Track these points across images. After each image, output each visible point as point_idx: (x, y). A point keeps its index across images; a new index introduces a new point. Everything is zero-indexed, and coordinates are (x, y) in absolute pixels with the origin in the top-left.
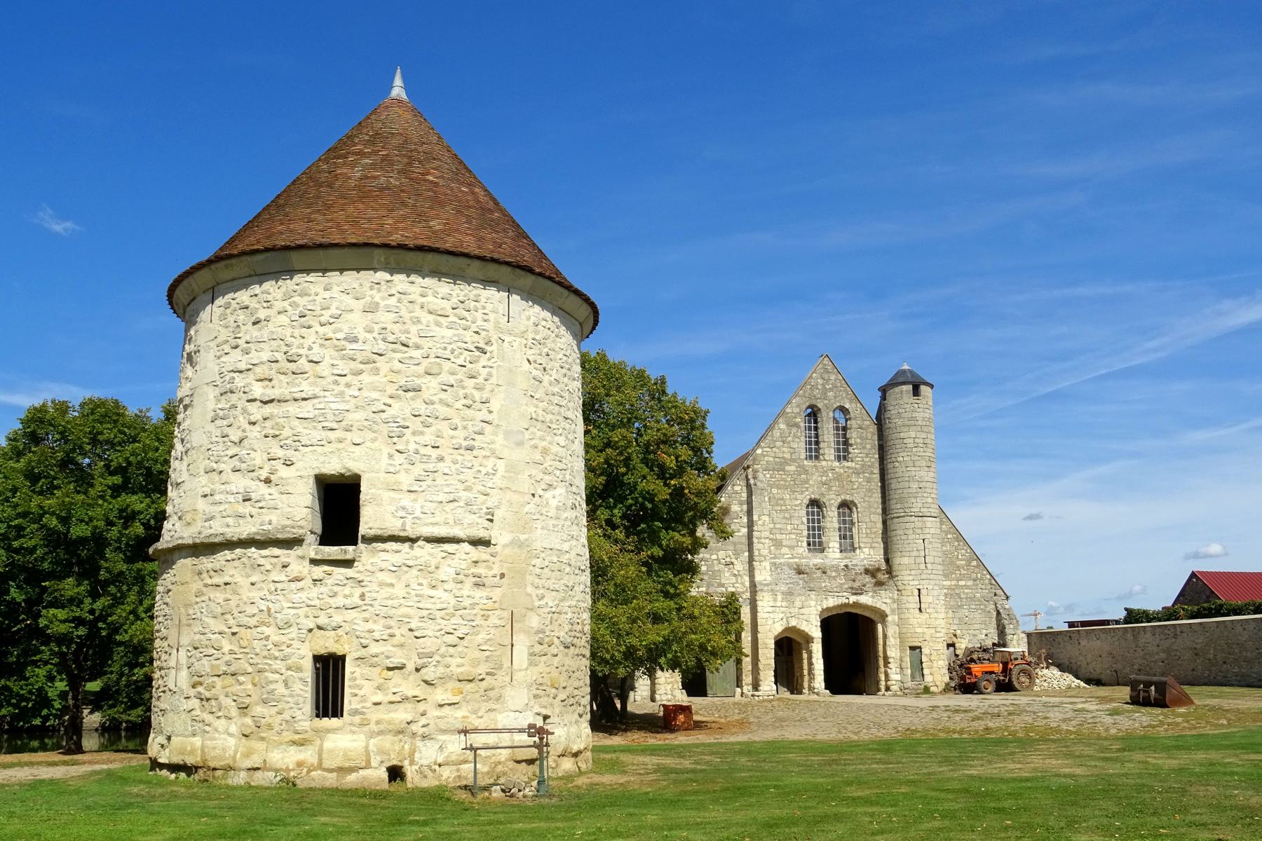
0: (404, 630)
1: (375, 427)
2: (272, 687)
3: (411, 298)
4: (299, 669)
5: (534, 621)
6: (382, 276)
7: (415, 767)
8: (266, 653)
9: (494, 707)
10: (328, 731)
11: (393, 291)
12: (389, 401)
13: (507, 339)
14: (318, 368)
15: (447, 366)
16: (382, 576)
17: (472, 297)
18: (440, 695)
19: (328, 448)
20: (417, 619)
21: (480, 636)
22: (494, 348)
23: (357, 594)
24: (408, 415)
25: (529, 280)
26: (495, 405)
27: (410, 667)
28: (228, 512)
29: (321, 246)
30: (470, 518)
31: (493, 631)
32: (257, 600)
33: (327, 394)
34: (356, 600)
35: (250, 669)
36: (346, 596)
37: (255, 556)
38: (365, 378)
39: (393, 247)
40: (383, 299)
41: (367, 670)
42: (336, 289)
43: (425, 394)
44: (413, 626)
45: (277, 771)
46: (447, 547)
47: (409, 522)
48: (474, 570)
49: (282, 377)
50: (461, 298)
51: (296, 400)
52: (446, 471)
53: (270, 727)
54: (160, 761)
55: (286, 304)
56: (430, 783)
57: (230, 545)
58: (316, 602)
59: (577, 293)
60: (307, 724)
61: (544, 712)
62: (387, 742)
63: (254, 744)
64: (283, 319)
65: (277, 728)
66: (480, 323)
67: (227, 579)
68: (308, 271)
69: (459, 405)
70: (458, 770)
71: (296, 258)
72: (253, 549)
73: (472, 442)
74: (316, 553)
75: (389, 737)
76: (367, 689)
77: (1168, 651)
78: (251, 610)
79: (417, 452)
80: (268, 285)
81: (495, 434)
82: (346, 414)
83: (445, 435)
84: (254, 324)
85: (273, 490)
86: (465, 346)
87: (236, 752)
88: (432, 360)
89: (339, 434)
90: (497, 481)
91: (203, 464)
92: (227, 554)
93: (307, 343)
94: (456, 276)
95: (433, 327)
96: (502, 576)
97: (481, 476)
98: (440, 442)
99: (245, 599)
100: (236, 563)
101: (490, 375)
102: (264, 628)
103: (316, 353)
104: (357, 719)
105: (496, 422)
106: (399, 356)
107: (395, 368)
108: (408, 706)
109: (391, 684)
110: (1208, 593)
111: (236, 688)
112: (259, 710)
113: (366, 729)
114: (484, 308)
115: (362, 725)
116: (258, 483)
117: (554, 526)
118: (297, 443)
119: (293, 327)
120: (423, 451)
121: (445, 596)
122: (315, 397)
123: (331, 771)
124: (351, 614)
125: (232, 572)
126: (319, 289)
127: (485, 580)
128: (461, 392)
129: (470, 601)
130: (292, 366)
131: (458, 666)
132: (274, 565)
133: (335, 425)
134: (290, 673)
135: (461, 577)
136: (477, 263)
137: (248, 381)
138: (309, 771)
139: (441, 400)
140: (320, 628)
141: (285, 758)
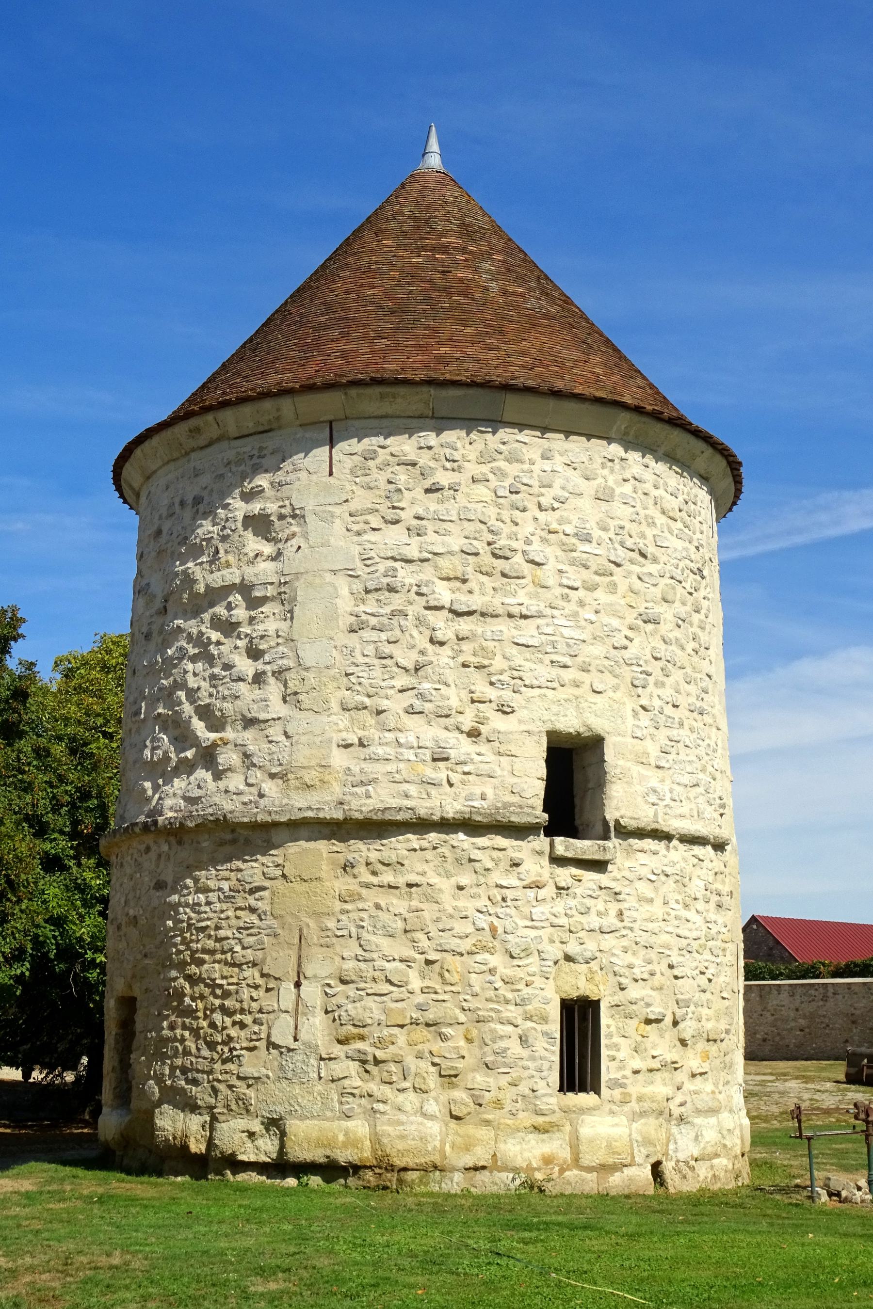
0: (664, 967)
1: (618, 671)
2: (503, 1044)
4: (544, 1019)
6: (616, 450)
8: (492, 993)
10: (583, 1111)
11: (628, 475)
12: (630, 634)
14: (539, 571)
23: (613, 913)
28: (405, 775)
29: (556, 394)
33: (556, 612)
34: (611, 921)
35: (462, 1018)
37: (466, 846)
45: (516, 1170)
47: (661, 810)
49: (484, 579)
51: (510, 616)
53: (498, 1104)
54: (242, 1157)
55: (485, 469)
56: (690, 1186)
57: (421, 825)
58: (563, 921)
60: (553, 1100)
62: (650, 1126)
63: (469, 1129)
64: (482, 491)
67: (413, 878)
68: (521, 426)
70: (712, 1167)
71: (512, 404)
72: (461, 836)
74: (567, 848)
75: (652, 1121)
77: (812, 1017)
78: (461, 927)
80: (451, 436)
82: (583, 646)
84: (428, 491)
85: (484, 748)
87: (443, 1143)
89: (567, 675)
91: (335, 697)
92: (413, 840)
99: (451, 911)
100: (429, 855)
102: (487, 956)
103: (536, 550)
104: (617, 1093)
106: (636, 569)
110: (771, 943)
111: (437, 1046)
112: (480, 1079)
113: (626, 1108)
116: (456, 734)
119: (499, 506)
122: (540, 615)
123: (589, 1169)
124: (608, 942)
125: (420, 867)
126: (535, 455)
130: (500, 564)
132: (497, 862)
133: (567, 660)
134: (529, 1024)
137: (423, 577)
138: (562, 1171)
140: (568, 958)
141: (526, 1151)
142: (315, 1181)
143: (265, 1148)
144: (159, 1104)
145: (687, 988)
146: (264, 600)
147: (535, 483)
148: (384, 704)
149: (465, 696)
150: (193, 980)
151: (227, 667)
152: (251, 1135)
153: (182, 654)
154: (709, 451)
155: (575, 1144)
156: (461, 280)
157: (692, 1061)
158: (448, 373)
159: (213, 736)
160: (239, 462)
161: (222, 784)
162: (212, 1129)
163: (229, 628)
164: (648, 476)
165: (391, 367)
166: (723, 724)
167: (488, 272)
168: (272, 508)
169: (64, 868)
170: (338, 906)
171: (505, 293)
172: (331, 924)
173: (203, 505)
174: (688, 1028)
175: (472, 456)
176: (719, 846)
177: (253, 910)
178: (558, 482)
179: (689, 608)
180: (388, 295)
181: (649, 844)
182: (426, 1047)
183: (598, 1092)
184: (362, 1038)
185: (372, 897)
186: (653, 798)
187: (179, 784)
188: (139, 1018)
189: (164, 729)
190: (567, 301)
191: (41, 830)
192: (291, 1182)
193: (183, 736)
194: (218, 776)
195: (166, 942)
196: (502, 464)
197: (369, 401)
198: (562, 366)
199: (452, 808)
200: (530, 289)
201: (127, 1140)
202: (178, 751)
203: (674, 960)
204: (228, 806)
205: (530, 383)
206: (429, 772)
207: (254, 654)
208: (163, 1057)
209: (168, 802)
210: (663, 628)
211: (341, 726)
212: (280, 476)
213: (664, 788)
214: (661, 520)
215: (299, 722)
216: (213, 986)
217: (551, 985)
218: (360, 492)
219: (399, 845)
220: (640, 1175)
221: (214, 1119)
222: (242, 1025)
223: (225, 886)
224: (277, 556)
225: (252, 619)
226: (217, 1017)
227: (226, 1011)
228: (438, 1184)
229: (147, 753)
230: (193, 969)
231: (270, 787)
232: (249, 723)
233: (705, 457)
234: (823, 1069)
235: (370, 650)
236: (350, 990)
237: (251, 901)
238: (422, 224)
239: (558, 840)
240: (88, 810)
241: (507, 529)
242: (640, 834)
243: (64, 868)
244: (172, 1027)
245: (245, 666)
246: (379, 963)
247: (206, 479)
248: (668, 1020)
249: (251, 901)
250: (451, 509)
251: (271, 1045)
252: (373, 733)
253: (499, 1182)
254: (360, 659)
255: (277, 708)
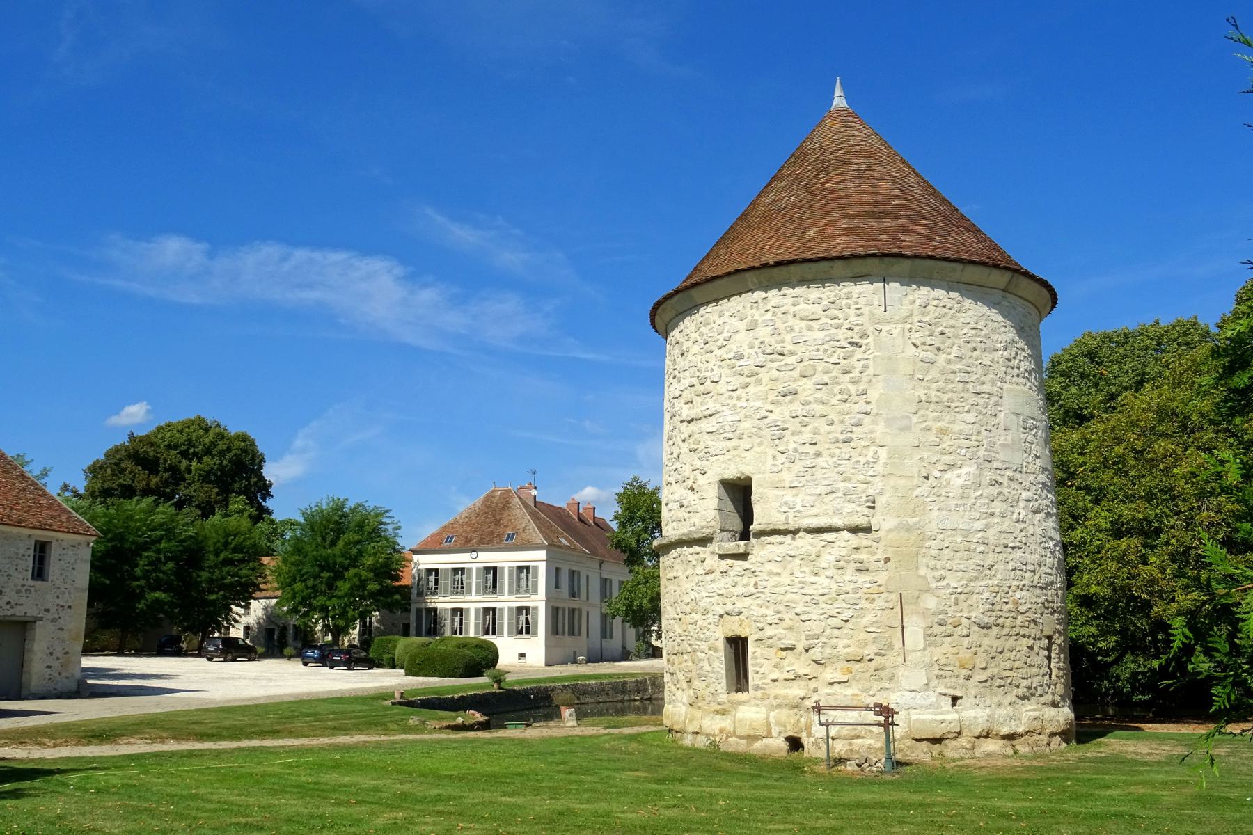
0: (792, 615)
1: (761, 433)
3: (783, 309)
5: (931, 603)
6: (759, 294)
7: (812, 739)
9: (887, 686)
10: (740, 703)
13: (885, 328)
14: (718, 386)
15: (820, 366)
16: (769, 567)
17: (843, 295)
18: (829, 674)
19: (727, 457)
20: (801, 604)
21: (865, 619)
22: (870, 339)
24: (788, 417)
25: (906, 264)
26: (873, 395)
27: (800, 647)
30: (849, 507)
31: (879, 613)
34: (752, 589)
36: (744, 586)
38: (752, 390)
39: (758, 268)
40: (761, 315)
41: (765, 651)
42: (727, 314)
43: (802, 396)
44: (798, 610)
45: (708, 735)
46: (826, 536)
47: (791, 515)
48: (855, 556)
50: (831, 299)
52: (824, 465)
58: (723, 591)
61: (953, 692)
62: (784, 714)
65: (707, 699)
66: (853, 318)
68: (706, 304)
69: (835, 401)
70: (850, 744)
73: (850, 435)
75: (785, 711)
76: (766, 667)
79: (796, 451)
81: (874, 423)
83: (822, 431)
85: (696, 497)
86: (837, 344)
88: (806, 363)
90: (879, 468)
94: (823, 280)
95: (805, 332)
96: (887, 560)
97: (860, 466)
98: (817, 438)
101: (866, 367)
104: (759, 693)
105: (875, 411)
106: (776, 365)
107: (774, 377)
108: (802, 683)
109: (785, 663)
113: (766, 702)
114: (857, 303)
115: (763, 699)
117: (957, 506)
118: (707, 455)
120: (801, 449)
121: (826, 582)
123: (742, 738)
124: (748, 601)
127: (867, 565)
128: (837, 389)
129: (853, 586)
131: (845, 647)
135: (842, 564)
136: (839, 263)
139: (816, 399)
141: (713, 724)
220: (777, 744)
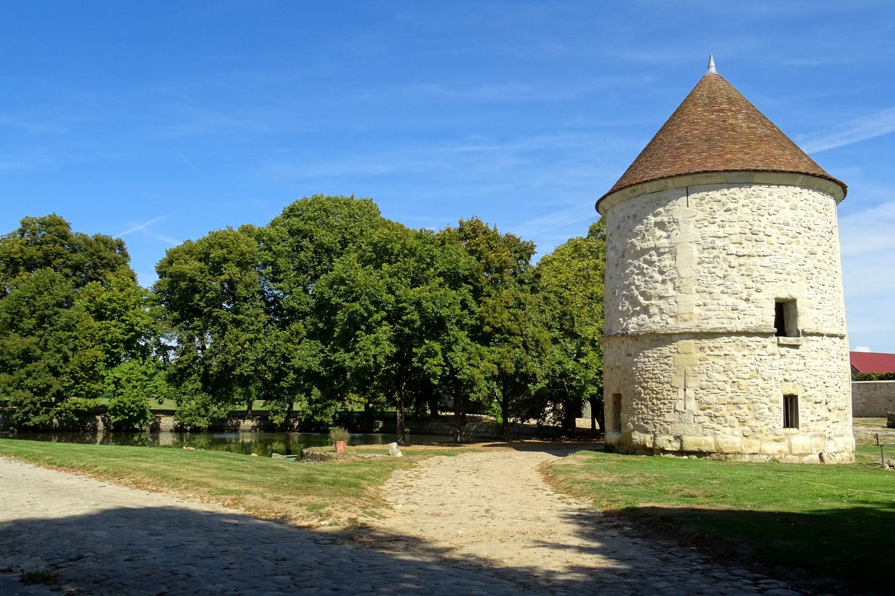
4: (777, 402)
6: (798, 189)
10: (792, 434)
19: (780, 284)
32: (749, 364)
34: (801, 367)
35: (747, 401)
45: (768, 455)
53: (761, 432)
55: (747, 201)
57: (729, 334)
59: (834, 181)
62: (818, 440)
63: (751, 440)
68: (760, 184)
71: (757, 177)
77: (868, 398)
78: (745, 370)
80: (733, 190)
85: (751, 305)
91: (694, 288)
92: (726, 339)
93: (762, 224)
100: (732, 344)
104: (805, 428)
106: (807, 235)
111: (738, 411)
112: (754, 423)
123: (796, 455)
124: (801, 374)
125: (729, 348)
132: (757, 346)
133: (782, 271)
140: (786, 380)
141: (772, 448)
142: (694, 457)
143: (676, 446)
144: (633, 431)
145: (831, 391)
146: (664, 253)
147: (767, 205)
148: (712, 290)
149: (743, 286)
150: (644, 388)
151: (651, 277)
152: (670, 441)
153: (632, 272)
154: (834, 185)
155: (790, 447)
156: (731, 124)
157: (833, 417)
158: (731, 167)
159: (647, 302)
160: (651, 202)
161: (652, 320)
162: (655, 439)
163: (651, 263)
164: (810, 198)
165: (709, 166)
166: (841, 289)
167: (741, 119)
168: (665, 219)
169: (558, 342)
170: (699, 362)
171: (749, 128)
172: (696, 369)
173: (638, 219)
174: (831, 405)
175: (742, 197)
176: (842, 337)
177: (666, 364)
178: (776, 204)
179: (828, 247)
180: (703, 133)
181: (815, 338)
182: (734, 412)
183: (798, 428)
184: (710, 408)
185: (711, 359)
186: (816, 321)
187: (634, 319)
188: (623, 402)
189: (626, 299)
190: (773, 126)
191: (550, 328)
192: (685, 457)
193: (634, 302)
194: (650, 316)
195: (633, 374)
196: (754, 199)
197: (702, 179)
198: (774, 157)
199: (740, 327)
200: (758, 124)
201: (620, 443)
202: (633, 308)
203: (826, 380)
204: (655, 327)
205: (764, 168)
206: (731, 314)
207: (661, 272)
208: (634, 415)
209: (630, 326)
210: (818, 256)
211: (696, 298)
212: (667, 207)
213: (820, 317)
214: (816, 214)
215: (681, 297)
216: (653, 390)
217: (779, 390)
218: (699, 212)
219: (720, 341)
221: (655, 436)
222: (665, 404)
223: (655, 355)
224: (668, 237)
225: (660, 260)
226: (655, 401)
227: (657, 399)
228: (739, 459)
229: (620, 308)
230: (644, 384)
231: (670, 320)
232: (661, 298)
233: (833, 187)
234: (875, 421)
235: (706, 270)
236: (705, 392)
237: (666, 361)
238: (712, 100)
239: (781, 338)
240: (567, 320)
241: (757, 223)
242: (812, 334)
243: (558, 342)
244: (637, 404)
245: (659, 277)
246: (715, 382)
247: (638, 208)
248: (824, 402)
249: (666, 361)
250: (735, 217)
251: (675, 411)
252: (709, 301)
253: (764, 458)
254: (702, 274)
255: (672, 292)
